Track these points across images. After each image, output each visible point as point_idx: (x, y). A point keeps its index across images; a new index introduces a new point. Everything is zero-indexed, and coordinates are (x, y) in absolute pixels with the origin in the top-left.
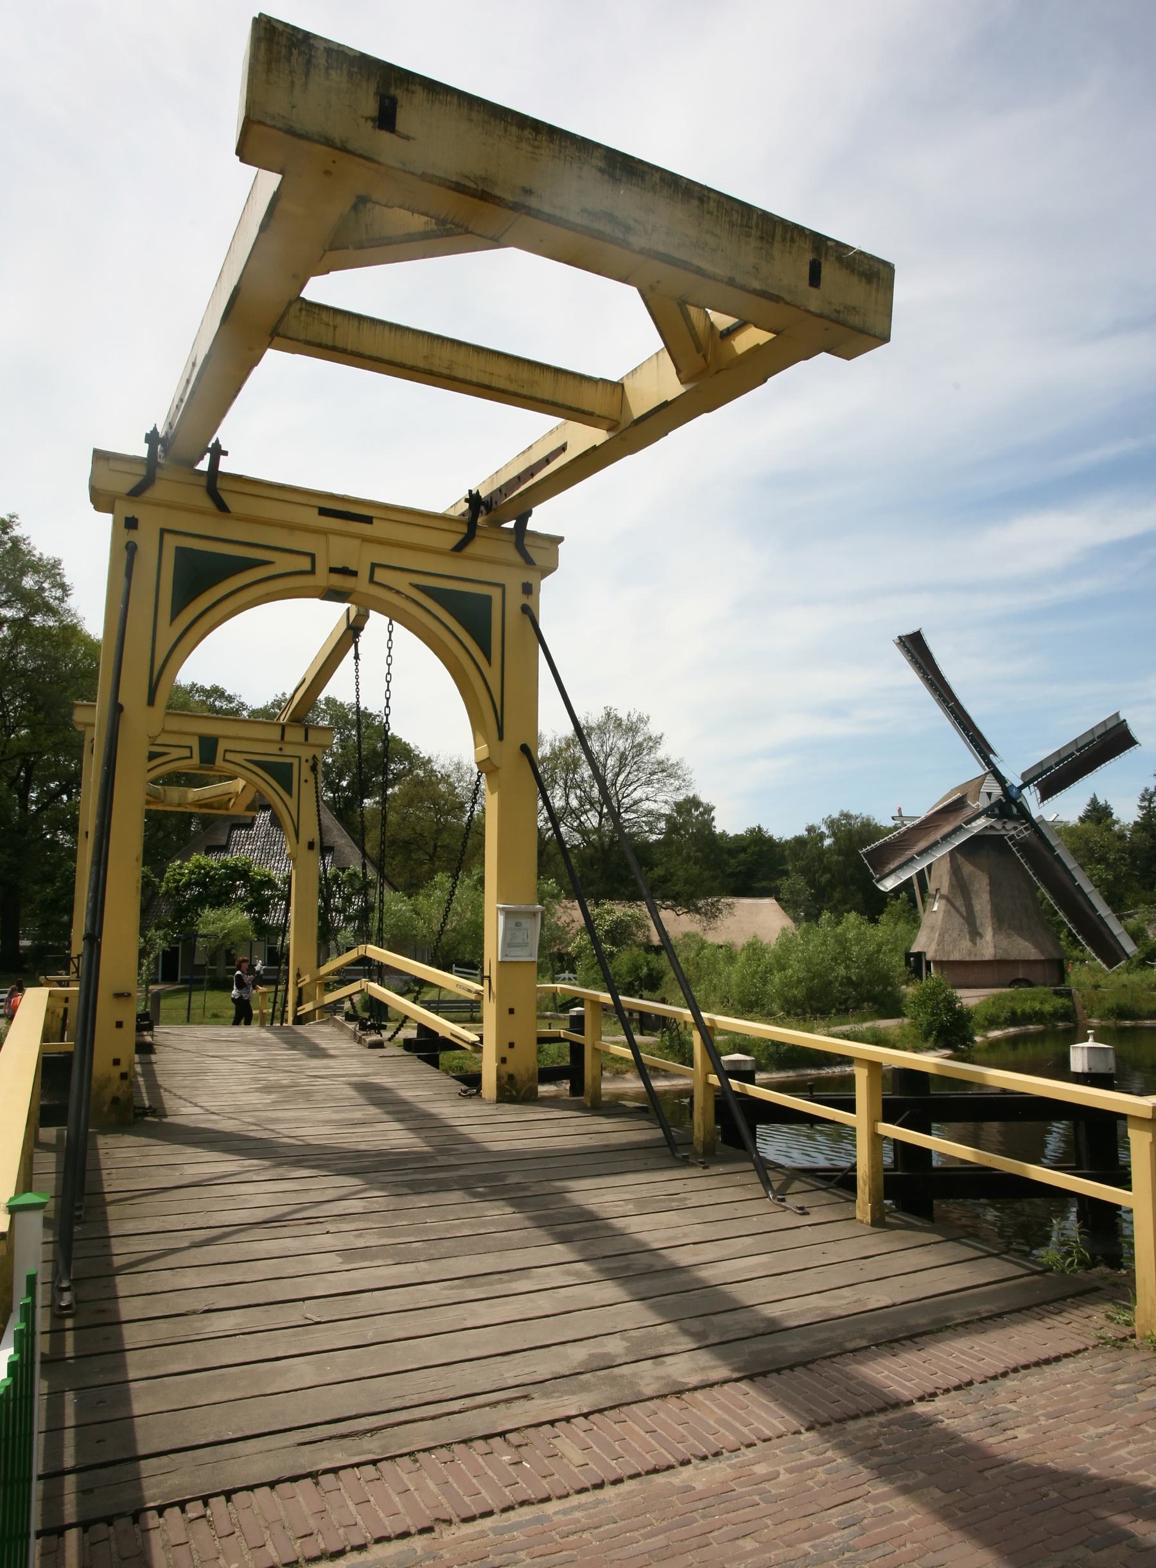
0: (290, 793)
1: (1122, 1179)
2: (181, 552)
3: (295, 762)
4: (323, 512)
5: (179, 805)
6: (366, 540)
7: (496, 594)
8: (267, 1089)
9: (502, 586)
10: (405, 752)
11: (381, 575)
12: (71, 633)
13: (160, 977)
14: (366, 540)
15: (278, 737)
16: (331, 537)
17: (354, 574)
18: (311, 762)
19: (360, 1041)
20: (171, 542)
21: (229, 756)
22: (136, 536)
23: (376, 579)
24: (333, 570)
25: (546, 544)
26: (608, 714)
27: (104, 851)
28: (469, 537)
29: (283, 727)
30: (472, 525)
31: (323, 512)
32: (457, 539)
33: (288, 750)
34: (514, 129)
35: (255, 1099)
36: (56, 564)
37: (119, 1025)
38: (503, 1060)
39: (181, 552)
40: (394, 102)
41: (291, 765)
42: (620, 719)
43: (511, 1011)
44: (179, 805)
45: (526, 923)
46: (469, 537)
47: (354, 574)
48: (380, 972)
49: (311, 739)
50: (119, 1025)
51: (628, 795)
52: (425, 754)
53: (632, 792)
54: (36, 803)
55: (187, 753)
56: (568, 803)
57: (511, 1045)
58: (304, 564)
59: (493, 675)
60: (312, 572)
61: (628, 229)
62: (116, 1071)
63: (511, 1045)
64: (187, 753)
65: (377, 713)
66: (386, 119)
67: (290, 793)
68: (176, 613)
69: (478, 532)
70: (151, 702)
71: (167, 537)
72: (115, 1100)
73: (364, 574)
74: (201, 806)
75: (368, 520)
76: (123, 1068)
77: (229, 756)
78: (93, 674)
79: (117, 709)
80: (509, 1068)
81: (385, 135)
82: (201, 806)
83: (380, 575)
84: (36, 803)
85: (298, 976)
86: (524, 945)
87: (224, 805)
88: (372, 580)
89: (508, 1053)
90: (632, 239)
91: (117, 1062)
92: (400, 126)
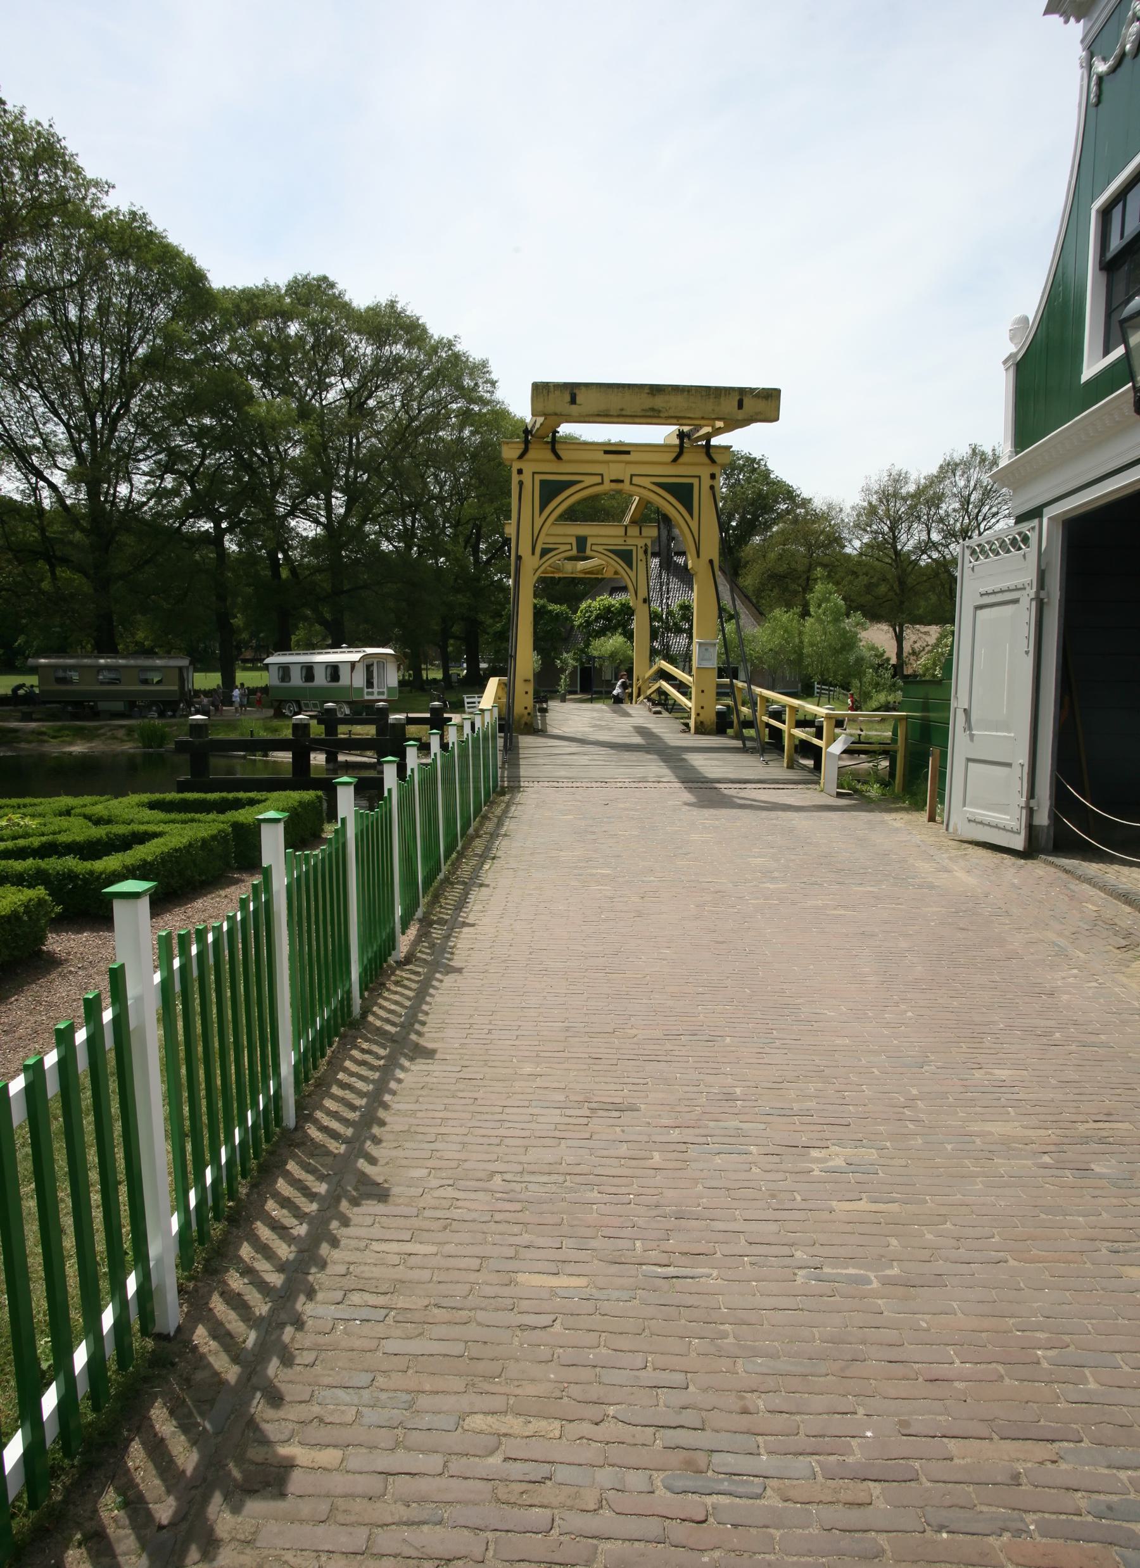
0: (631, 568)
1: (784, 722)
2: (542, 482)
3: (634, 548)
4: (606, 452)
5: (572, 573)
6: (628, 463)
7: (695, 481)
8: (593, 727)
9: (699, 477)
10: (789, 494)
11: (636, 480)
12: (500, 416)
13: (579, 689)
14: (628, 463)
15: (623, 534)
16: (611, 464)
17: (622, 481)
18: (644, 548)
19: (650, 710)
20: (538, 478)
21: (594, 548)
22: (522, 477)
23: (633, 482)
24: (612, 481)
25: (723, 451)
26: (974, 450)
27: (295, 911)
28: (680, 454)
29: (626, 527)
30: (681, 446)
31: (606, 452)
32: (674, 455)
33: (630, 541)
34: (616, 390)
35: (587, 729)
36: (484, 364)
37: (527, 693)
38: (698, 715)
39: (542, 482)
40: (575, 395)
41: (632, 550)
42: (983, 453)
43: (703, 691)
44: (572, 573)
45: (711, 649)
46: (680, 454)
47: (622, 481)
48: (669, 677)
49: (644, 534)
50: (527, 693)
51: (990, 528)
52: (806, 494)
53: (994, 524)
54: (486, 552)
55: (569, 547)
56: (929, 538)
57: (702, 708)
58: (598, 479)
59: (694, 525)
60: (602, 483)
61: (660, 411)
62: (526, 712)
63: (702, 708)
64: (569, 547)
65: (761, 457)
66: (573, 401)
67: (631, 568)
68: (542, 510)
69: (685, 450)
70: (533, 553)
71: (536, 476)
72: (526, 724)
73: (627, 481)
74: (586, 573)
75: (628, 453)
76: (529, 710)
77: (594, 548)
78: (510, 539)
79: (519, 558)
80: (701, 718)
81: (574, 406)
82: (586, 573)
83: (636, 480)
84: (486, 552)
85: (638, 680)
86: (709, 660)
87: (600, 571)
88: (631, 483)
89: (700, 711)
90: (661, 415)
91: (526, 708)
92: (578, 402)
